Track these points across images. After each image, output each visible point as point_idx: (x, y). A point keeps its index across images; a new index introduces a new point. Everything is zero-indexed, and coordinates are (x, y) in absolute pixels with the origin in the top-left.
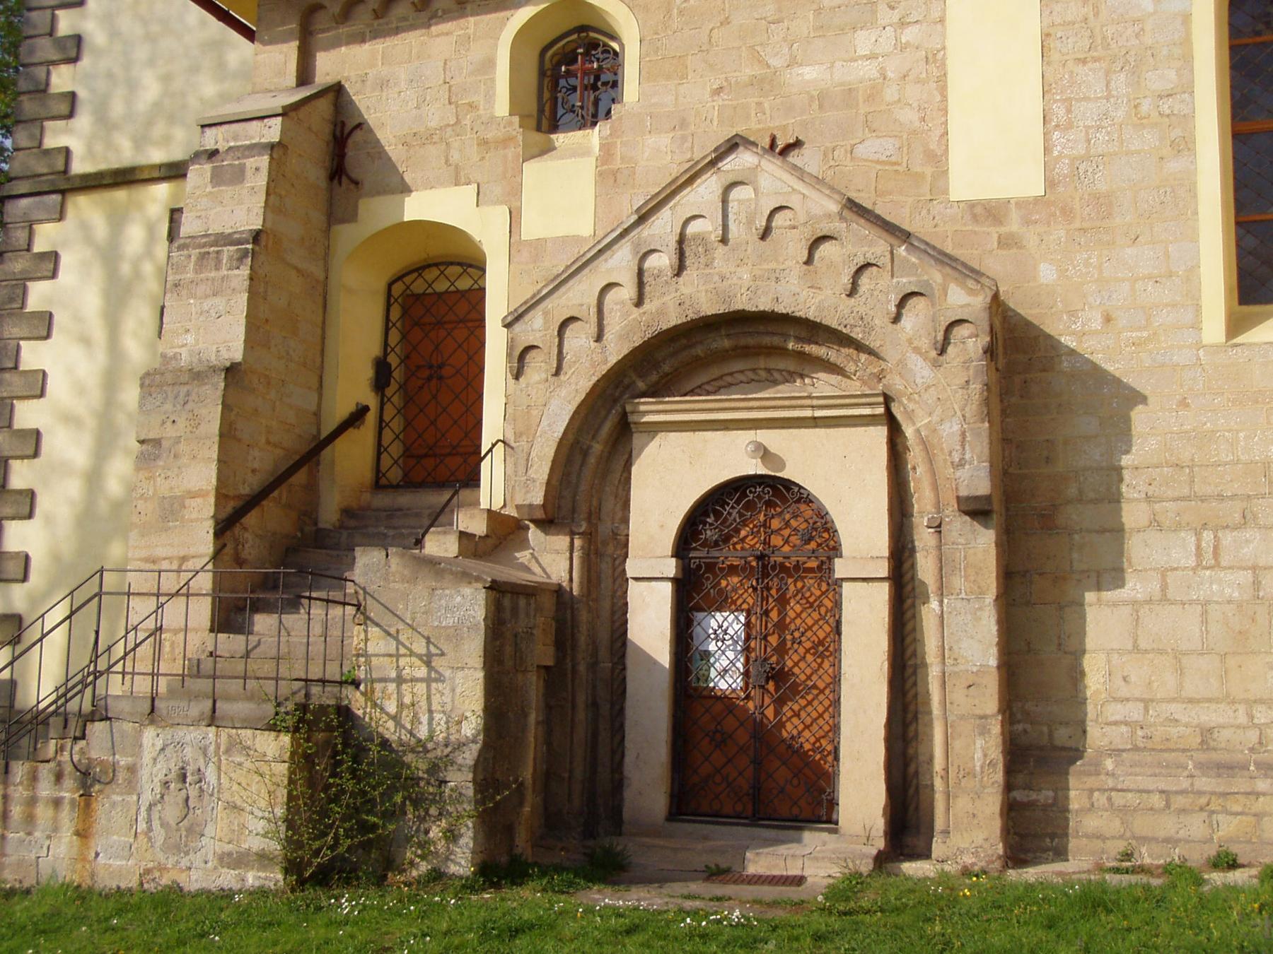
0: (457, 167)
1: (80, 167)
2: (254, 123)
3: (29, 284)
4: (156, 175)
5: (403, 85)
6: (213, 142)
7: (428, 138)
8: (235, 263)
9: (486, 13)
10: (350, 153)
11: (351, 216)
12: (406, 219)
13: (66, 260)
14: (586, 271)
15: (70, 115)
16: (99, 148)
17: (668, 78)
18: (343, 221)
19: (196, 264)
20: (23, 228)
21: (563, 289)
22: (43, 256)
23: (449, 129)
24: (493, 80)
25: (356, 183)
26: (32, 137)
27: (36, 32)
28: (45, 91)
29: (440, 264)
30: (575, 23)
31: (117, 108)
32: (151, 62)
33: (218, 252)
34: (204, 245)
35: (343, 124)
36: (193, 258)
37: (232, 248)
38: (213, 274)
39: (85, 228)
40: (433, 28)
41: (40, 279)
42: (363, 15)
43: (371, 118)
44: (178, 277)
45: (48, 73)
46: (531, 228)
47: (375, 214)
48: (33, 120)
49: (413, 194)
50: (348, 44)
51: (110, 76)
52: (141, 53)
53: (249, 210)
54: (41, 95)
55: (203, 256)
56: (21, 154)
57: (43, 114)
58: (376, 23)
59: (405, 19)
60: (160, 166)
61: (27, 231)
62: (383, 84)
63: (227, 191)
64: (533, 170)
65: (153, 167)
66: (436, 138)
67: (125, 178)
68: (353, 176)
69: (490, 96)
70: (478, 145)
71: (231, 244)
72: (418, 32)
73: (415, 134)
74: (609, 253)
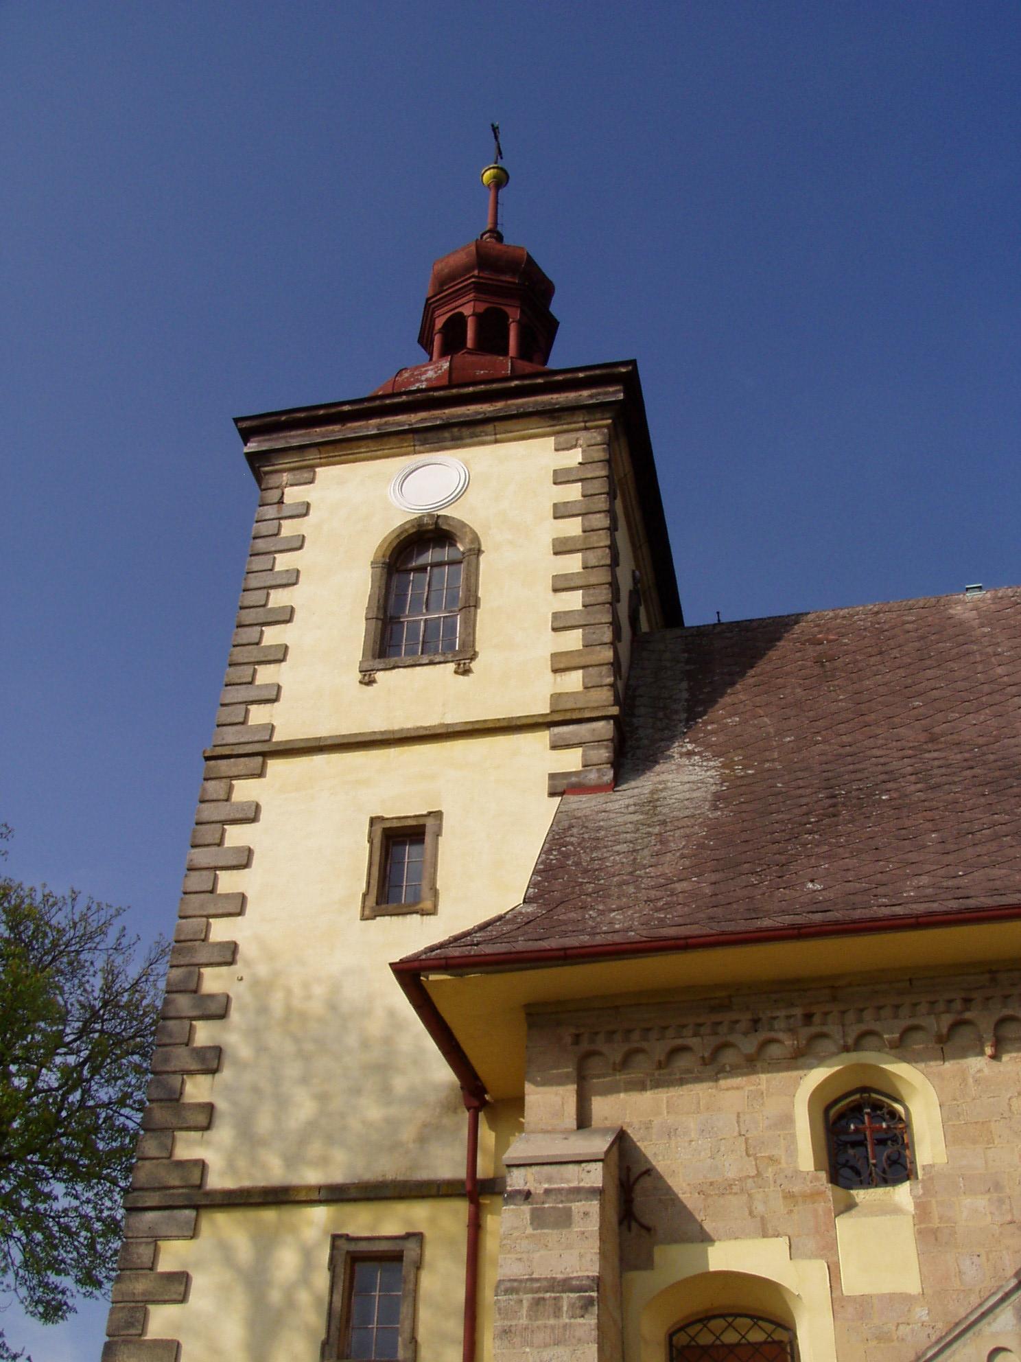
0: (762, 1218)
1: (217, 1181)
2: (571, 1167)
3: (151, 1308)
4: (315, 1196)
5: (693, 1135)
6: (522, 1182)
7: (727, 1188)
8: (578, 1312)
9: (779, 1071)
10: (639, 1198)
11: (647, 1263)
12: (712, 1269)
13: (199, 1282)
14: (969, 1335)
15: (207, 1127)
16: (242, 1163)
17: (974, 1142)
18: (636, 1268)
19: (530, 1309)
20: (148, 1243)
21: (947, 1353)
22: (172, 1277)
23: (750, 1180)
24: (793, 1136)
25: (648, 1229)
26: (162, 1146)
27: (172, 1041)
28: (178, 1100)
29: (730, 1314)
30: (858, 1085)
31: (264, 1123)
32: (304, 1080)
33: (555, 1298)
34: (538, 1290)
35: (629, 1169)
36: (525, 1304)
37: (572, 1295)
38: (552, 1322)
39: (226, 1252)
40: (722, 1083)
41: (165, 1302)
42: (643, 1065)
43: (660, 1165)
44: (507, 1323)
45: (183, 1082)
46: (852, 1284)
47: (673, 1262)
48: (163, 1129)
49: (717, 1244)
50: (626, 1090)
51: (256, 1090)
52: (293, 1070)
53: (581, 1256)
54: (175, 1104)
55: (538, 1302)
56: (147, 1163)
57: (174, 1122)
58: (657, 1073)
59: (689, 1071)
60: (319, 1188)
61: (152, 1247)
62: (671, 1132)
63: (551, 1235)
64: (844, 1225)
65: (309, 1188)
66: (735, 1189)
67: (279, 1197)
68: (646, 1220)
69: (792, 1150)
70: (785, 1198)
71: (572, 1290)
72: (705, 1085)
73: (711, 1184)
74: (991, 1316)
